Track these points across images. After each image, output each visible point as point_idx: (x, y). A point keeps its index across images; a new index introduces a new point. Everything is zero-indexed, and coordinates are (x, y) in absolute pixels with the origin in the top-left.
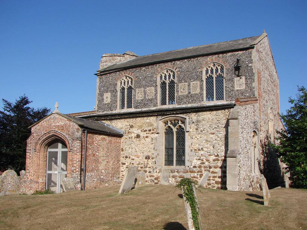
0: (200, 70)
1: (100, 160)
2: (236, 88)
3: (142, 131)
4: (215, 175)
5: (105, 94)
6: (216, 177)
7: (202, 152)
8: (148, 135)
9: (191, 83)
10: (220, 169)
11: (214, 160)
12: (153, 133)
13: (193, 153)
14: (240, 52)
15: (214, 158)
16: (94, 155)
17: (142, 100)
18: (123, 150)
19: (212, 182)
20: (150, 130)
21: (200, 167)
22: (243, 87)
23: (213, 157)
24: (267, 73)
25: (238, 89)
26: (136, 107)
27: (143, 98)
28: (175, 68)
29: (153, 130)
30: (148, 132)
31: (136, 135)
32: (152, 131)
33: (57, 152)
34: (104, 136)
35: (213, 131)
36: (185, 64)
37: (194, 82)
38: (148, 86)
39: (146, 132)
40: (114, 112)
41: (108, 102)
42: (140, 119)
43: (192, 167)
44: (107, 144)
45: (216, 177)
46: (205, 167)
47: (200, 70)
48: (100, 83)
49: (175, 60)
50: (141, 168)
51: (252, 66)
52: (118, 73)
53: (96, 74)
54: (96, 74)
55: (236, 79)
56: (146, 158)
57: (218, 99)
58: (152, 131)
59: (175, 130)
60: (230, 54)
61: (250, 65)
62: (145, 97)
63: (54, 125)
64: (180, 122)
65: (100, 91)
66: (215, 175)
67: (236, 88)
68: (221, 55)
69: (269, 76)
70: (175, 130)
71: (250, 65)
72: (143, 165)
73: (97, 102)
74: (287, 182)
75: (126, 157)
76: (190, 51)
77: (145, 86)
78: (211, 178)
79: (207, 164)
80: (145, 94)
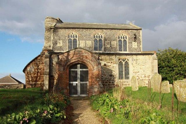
3: (107, 62)
4: (145, 83)
7: (138, 73)
8: (110, 64)
9: (112, 42)
10: (176, 83)
11: (144, 77)
12: (113, 64)
14: (135, 31)
15: (144, 76)
22: (136, 47)
27: (84, 46)
28: (103, 33)
29: (114, 62)
30: (111, 63)
33: (77, 71)
35: (144, 64)
37: (113, 42)
39: (109, 63)
41: (60, 46)
42: (138, 56)
49: (103, 29)
52: (67, 30)
55: (133, 43)
56: (110, 76)
57: (124, 51)
58: (113, 63)
59: (124, 63)
60: (131, 31)
61: (139, 37)
62: (86, 46)
64: (121, 60)
65: (54, 39)
66: (145, 83)
68: (126, 31)
70: (124, 63)
71: (139, 37)
72: (107, 80)
74: (82, 83)
77: (85, 40)
79: (141, 78)
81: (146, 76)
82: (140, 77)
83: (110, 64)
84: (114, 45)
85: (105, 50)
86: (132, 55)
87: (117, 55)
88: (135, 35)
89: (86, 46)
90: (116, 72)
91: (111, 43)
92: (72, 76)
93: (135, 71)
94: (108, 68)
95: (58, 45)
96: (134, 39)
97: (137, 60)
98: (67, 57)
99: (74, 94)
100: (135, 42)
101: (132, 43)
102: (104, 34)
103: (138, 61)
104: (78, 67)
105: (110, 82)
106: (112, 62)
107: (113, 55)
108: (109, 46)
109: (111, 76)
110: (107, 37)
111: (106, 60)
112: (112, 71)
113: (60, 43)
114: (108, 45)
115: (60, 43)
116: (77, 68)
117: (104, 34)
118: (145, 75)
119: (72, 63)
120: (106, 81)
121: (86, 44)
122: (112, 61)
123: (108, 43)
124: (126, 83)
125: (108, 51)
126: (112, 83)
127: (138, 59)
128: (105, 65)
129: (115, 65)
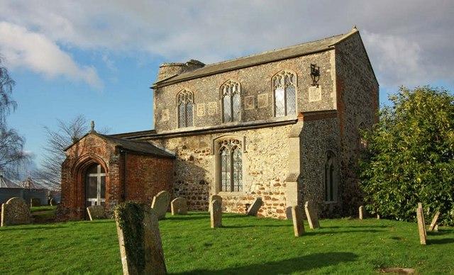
1: (146, 186)
2: (311, 101)
4: (276, 202)
6: (277, 205)
8: (202, 157)
12: (207, 155)
13: (251, 178)
16: (138, 180)
17: (204, 117)
18: (175, 174)
19: (273, 210)
20: (204, 152)
21: (259, 193)
22: (320, 99)
23: (274, 182)
24: (357, 82)
25: (313, 101)
26: (197, 125)
31: (189, 157)
32: (206, 153)
34: (150, 159)
38: (210, 101)
40: (173, 131)
43: (250, 193)
44: (155, 167)
45: (277, 205)
46: (265, 193)
50: (196, 194)
51: (329, 73)
52: (176, 85)
53: (152, 88)
54: (152, 88)
56: (200, 183)
58: (206, 153)
61: (328, 71)
62: (207, 113)
66: (276, 202)
67: (311, 101)
69: (361, 83)
71: (328, 71)
72: (197, 191)
73: (154, 120)
75: (180, 182)
76: (262, 56)
77: (206, 101)
78: (272, 206)
79: (267, 189)
81: (279, 182)
82: (264, 186)
83: (202, 157)
84: (262, 103)
85: (244, 119)
86: (244, 130)
87: (214, 133)
88: (313, 67)
90: (211, 175)
91: (256, 99)
92: (92, 188)
93: (253, 170)
94: (198, 165)
95: (164, 119)
96: (310, 80)
97: (256, 140)
98: (76, 153)
99: (439, 216)
100: (315, 87)
101: (306, 90)
103: (259, 144)
104: (97, 169)
105: (200, 198)
106: (204, 152)
107: (205, 134)
108: (252, 107)
109: (203, 182)
110: (247, 87)
111: (194, 147)
112: (204, 171)
113: (165, 115)
114: (250, 105)
115: (165, 115)
116: (96, 172)
118: (278, 180)
119: (83, 163)
120: (194, 195)
122: (205, 149)
123: (251, 99)
124: (232, 201)
125: (251, 120)
126: (205, 199)
127: (259, 137)
128: (192, 158)
129: (211, 157)
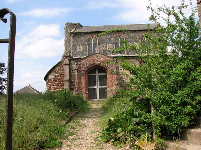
0: (138, 38)
5: (78, 46)
17: (105, 51)
27: (105, 50)
36: (132, 34)
38: (108, 44)
47: (138, 38)
48: (73, 40)
62: (106, 50)
63: (97, 59)
65: (73, 44)
77: (106, 44)
80: (106, 48)
89: (106, 50)
102: (125, 36)
117: (125, 36)
121: (106, 48)
